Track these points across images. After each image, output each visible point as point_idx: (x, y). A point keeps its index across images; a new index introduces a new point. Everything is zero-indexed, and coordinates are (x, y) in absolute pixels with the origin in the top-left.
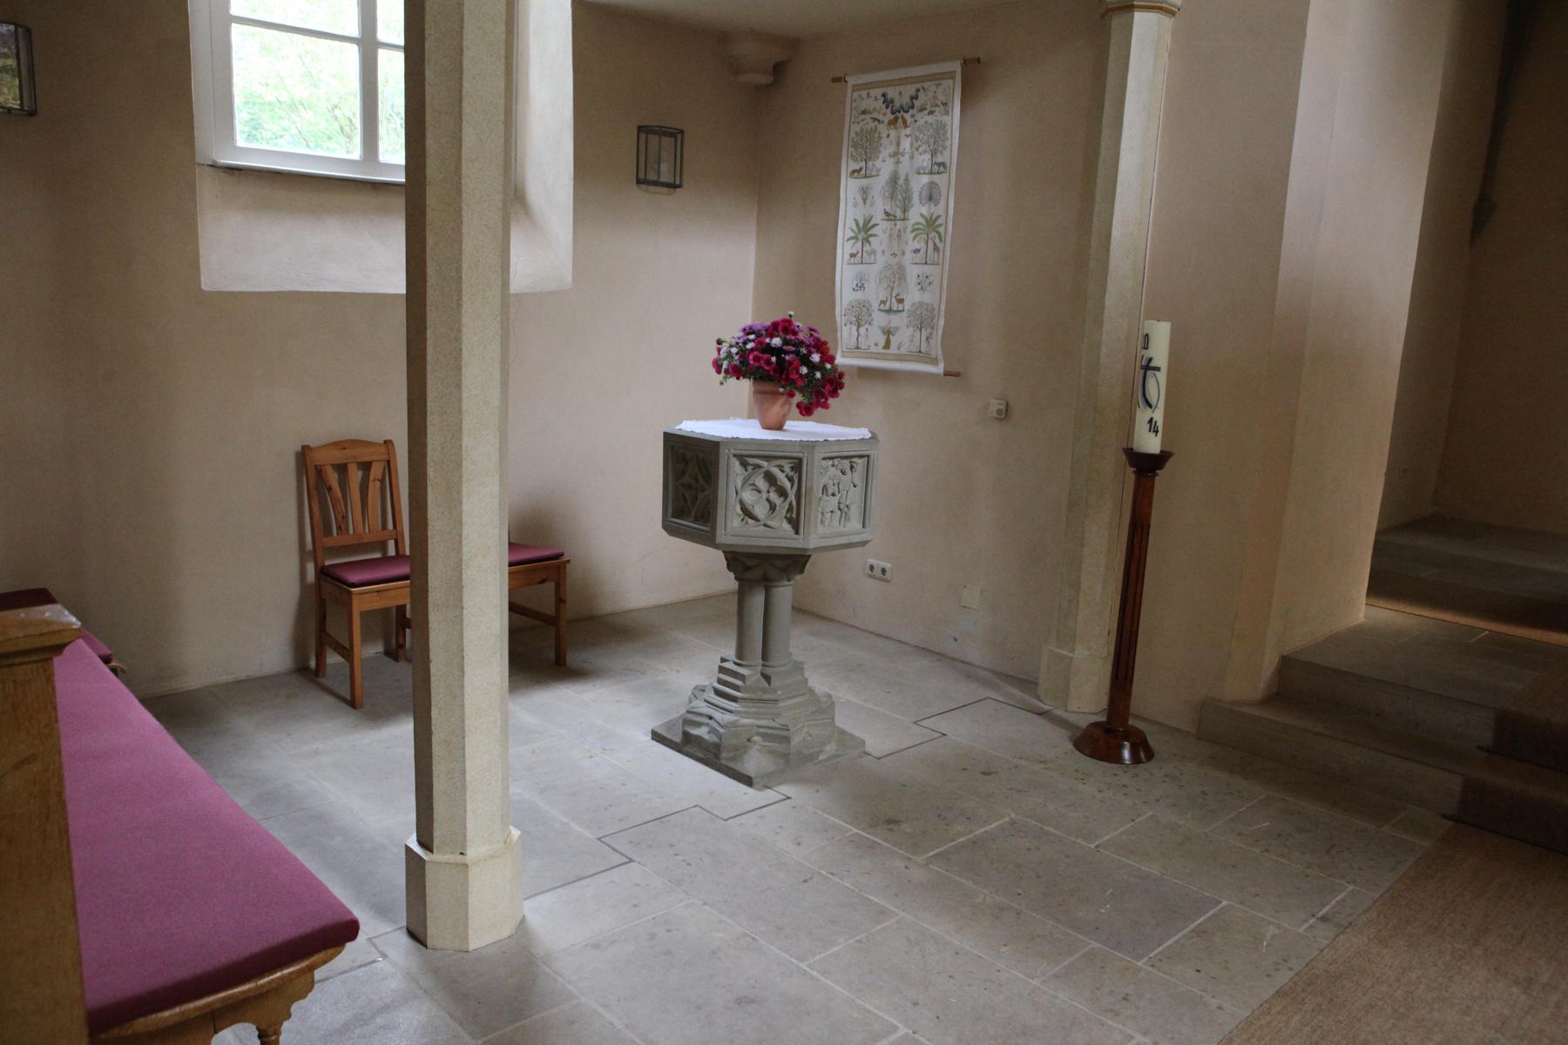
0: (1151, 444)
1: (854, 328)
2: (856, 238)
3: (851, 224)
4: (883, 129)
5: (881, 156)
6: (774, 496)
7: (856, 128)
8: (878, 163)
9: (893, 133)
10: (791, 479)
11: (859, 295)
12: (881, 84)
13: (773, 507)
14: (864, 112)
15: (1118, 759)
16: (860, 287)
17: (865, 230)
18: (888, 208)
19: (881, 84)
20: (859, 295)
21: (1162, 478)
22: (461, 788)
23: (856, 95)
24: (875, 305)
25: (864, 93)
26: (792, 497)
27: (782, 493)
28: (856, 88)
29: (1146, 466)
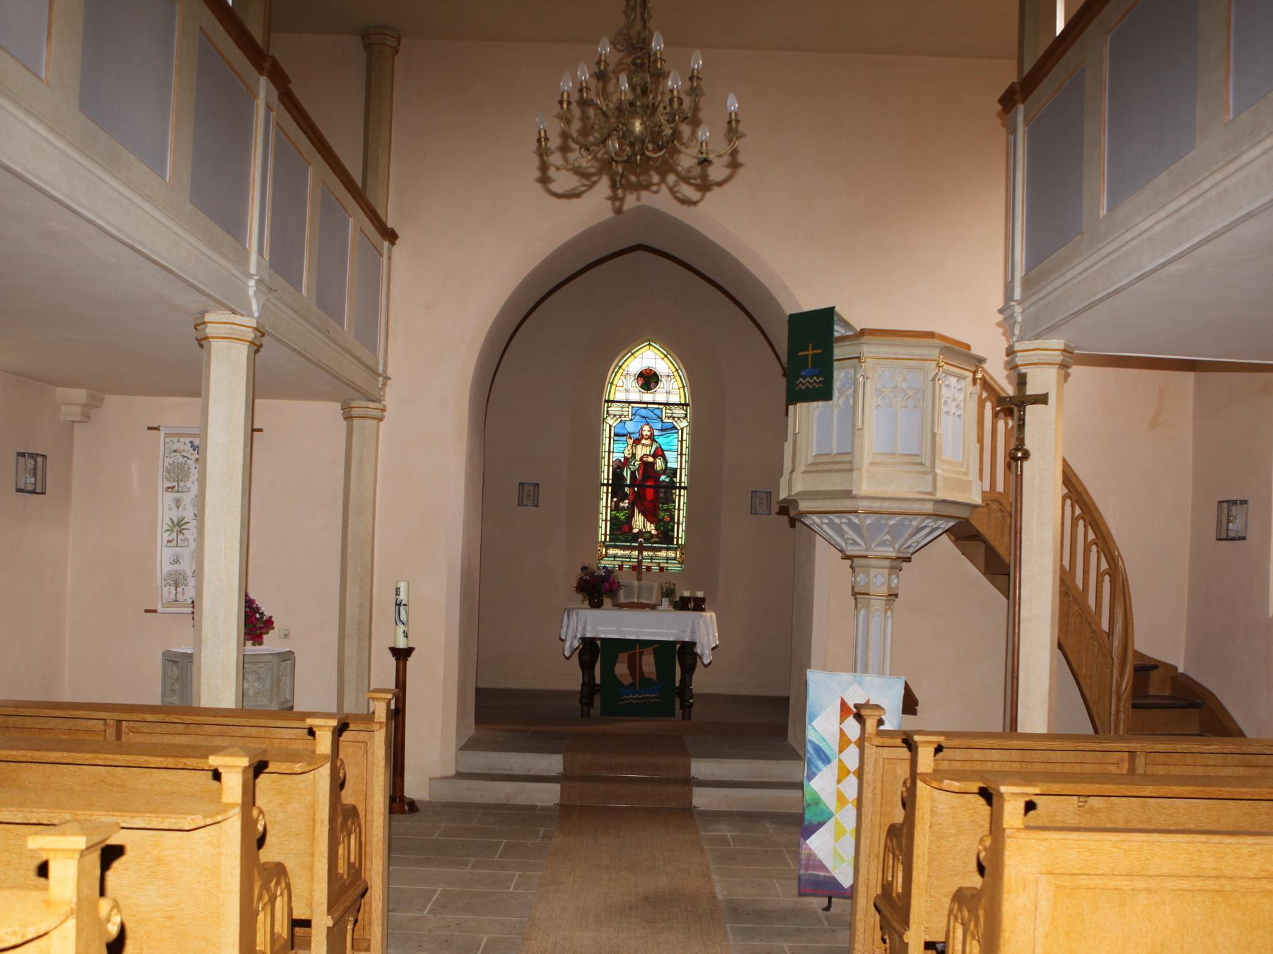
1: (173, 589)
2: (171, 530)
8: (188, 484)
11: (176, 567)
20: (176, 567)
25: (175, 440)
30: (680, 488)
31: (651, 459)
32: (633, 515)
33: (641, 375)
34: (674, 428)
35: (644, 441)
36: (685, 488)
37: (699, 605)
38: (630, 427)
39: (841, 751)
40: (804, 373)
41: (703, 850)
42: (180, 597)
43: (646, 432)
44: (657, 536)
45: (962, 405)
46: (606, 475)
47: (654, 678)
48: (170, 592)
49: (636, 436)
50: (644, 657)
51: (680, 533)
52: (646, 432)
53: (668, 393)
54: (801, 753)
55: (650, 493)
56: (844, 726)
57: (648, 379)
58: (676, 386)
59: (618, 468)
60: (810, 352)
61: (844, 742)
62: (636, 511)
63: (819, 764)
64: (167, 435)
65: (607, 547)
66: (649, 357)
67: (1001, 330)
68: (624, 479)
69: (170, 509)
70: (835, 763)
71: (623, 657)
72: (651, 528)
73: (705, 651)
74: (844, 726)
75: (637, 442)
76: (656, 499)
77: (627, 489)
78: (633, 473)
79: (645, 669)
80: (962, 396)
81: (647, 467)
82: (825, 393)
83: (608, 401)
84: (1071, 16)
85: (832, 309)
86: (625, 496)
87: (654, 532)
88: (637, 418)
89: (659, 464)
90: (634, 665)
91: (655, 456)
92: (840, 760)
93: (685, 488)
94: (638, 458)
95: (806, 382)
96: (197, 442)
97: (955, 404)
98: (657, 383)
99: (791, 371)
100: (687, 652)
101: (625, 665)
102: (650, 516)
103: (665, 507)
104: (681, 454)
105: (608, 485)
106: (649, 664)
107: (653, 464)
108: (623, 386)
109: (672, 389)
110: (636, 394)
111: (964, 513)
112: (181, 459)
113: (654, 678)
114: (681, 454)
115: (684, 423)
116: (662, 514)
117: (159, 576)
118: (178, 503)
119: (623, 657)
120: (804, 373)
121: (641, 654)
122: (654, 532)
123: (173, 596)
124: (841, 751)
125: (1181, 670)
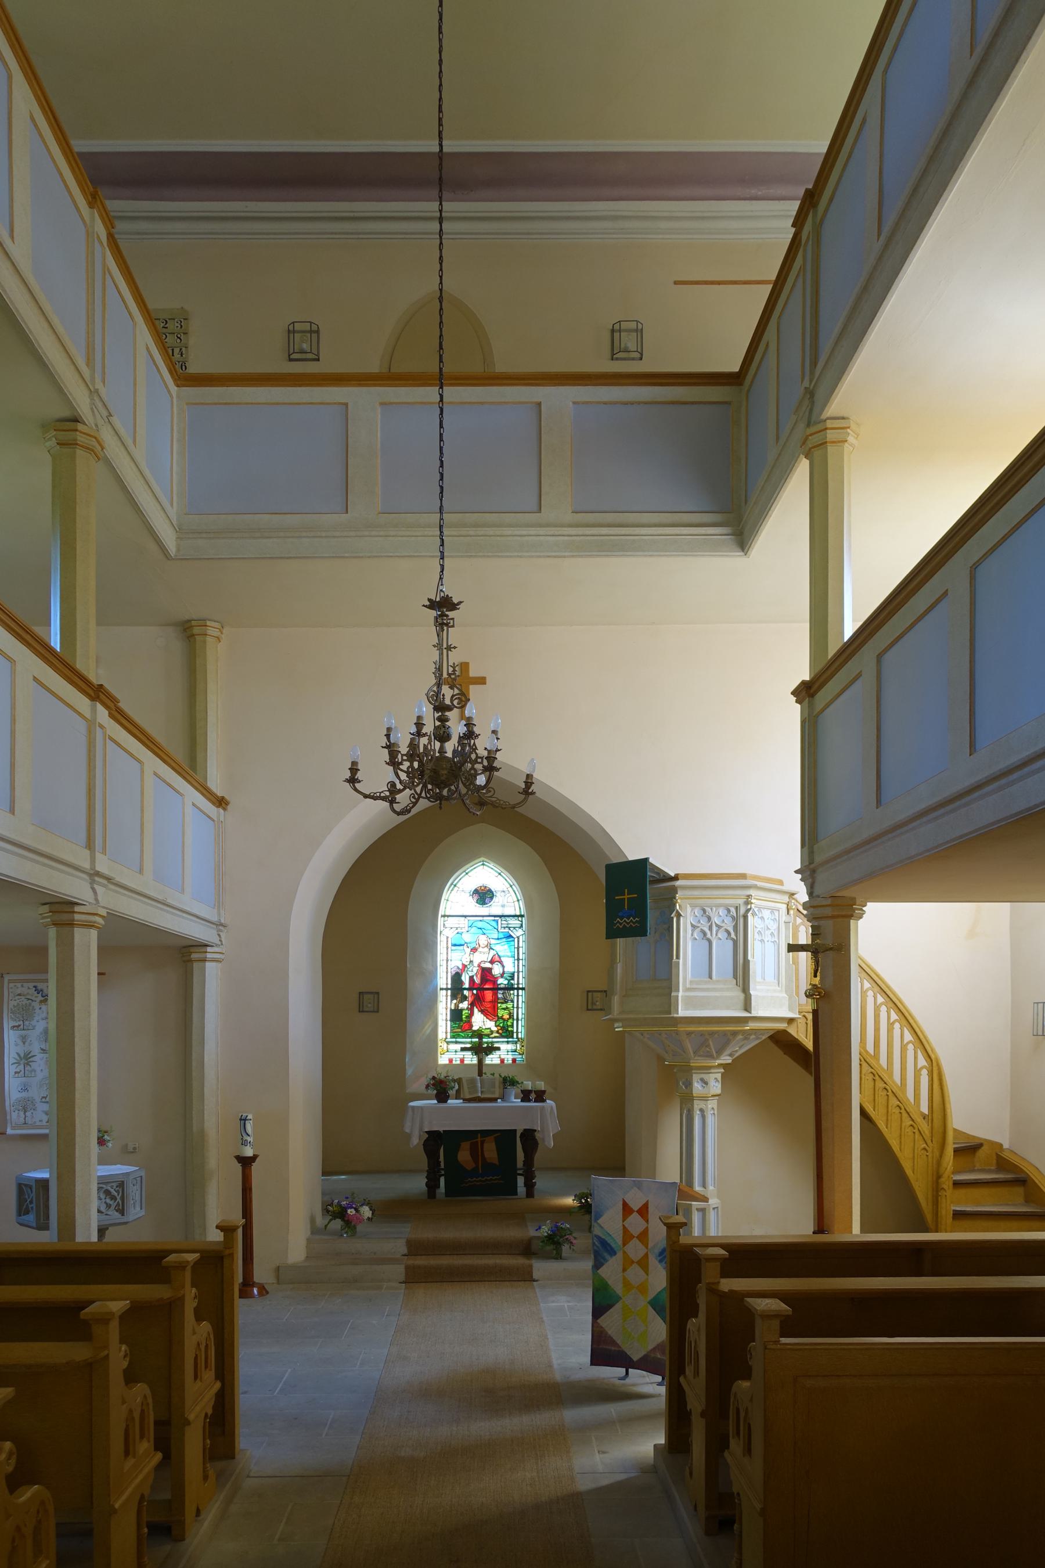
0: (249, 1152)
1: (22, 1113)
2: (18, 1063)
3: (13, 1055)
4: (36, 1005)
5: (36, 1018)
6: (108, 1201)
7: (13, 1003)
8: (34, 1023)
9: (44, 1007)
10: (118, 1192)
11: (24, 1094)
12: (33, 981)
13: (109, 1206)
14: (19, 995)
15: (252, 1296)
16: (25, 1089)
17: (26, 1059)
18: (43, 1047)
19: (33, 981)
20: (24, 1094)
21: (255, 1166)
22: (765, 1237)
23: (11, 985)
24: (38, 1100)
25: (19, 985)
26: (118, 1199)
27: (113, 1198)
28: (10, 981)
29: (246, 1162)
30: (518, 989)
31: (488, 965)
32: (472, 1014)
33: (476, 892)
34: (511, 936)
35: (480, 949)
36: (523, 989)
37: (540, 1096)
38: (467, 937)
39: (624, 1245)
40: (620, 914)
41: (541, 1321)
42: (29, 1120)
43: (483, 940)
44: (497, 1032)
45: (776, 934)
46: (443, 980)
47: (496, 1162)
48: (19, 1116)
49: (473, 946)
50: (486, 1146)
51: (520, 1029)
52: (483, 940)
53: (503, 906)
54: (978, 1142)
55: (489, 995)
56: (626, 1224)
57: (484, 895)
58: (510, 899)
59: (457, 978)
60: (626, 897)
61: (627, 1236)
62: (476, 1010)
63: (606, 1254)
64: (10, 981)
65: (448, 1043)
66: (483, 873)
67: (800, 876)
68: (462, 983)
69: (16, 1045)
70: (620, 1255)
71: (466, 1146)
72: (491, 1025)
73: (548, 1140)
74: (626, 1224)
75: (474, 950)
76: (495, 1001)
77: (466, 993)
78: (471, 978)
79: (487, 1155)
80: (775, 926)
81: (486, 973)
82: (640, 931)
83: (444, 916)
84: (820, 666)
85: (646, 860)
86: (465, 998)
87: (495, 1029)
88: (474, 930)
89: (497, 970)
90: (475, 1152)
91: (492, 962)
92: (624, 1252)
93: (523, 989)
94: (476, 964)
95: (621, 922)
96: (40, 986)
97: (768, 933)
98: (492, 898)
99: (613, 909)
100: (529, 1137)
101: (468, 1153)
102: (490, 1013)
103: (504, 1006)
104: (518, 959)
105: (447, 989)
106: (490, 1152)
107: (490, 970)
108: (456, 899)
109: (509, 898)
110: (472, 907)
111: (782, 1026)
112: (26, 1002)
113: (496, 1162)
114: (518, 959)
115: (520, 932)
116: (500, 1013)
117: (7, 1103)
118: (24, 1039)
119: (466, 1146)
120: (620, 914)
121: (482, 1143)
122: (495, 1029)
123: (22, 1120)
124: (624, 1245)
125: (1006, 1146)
